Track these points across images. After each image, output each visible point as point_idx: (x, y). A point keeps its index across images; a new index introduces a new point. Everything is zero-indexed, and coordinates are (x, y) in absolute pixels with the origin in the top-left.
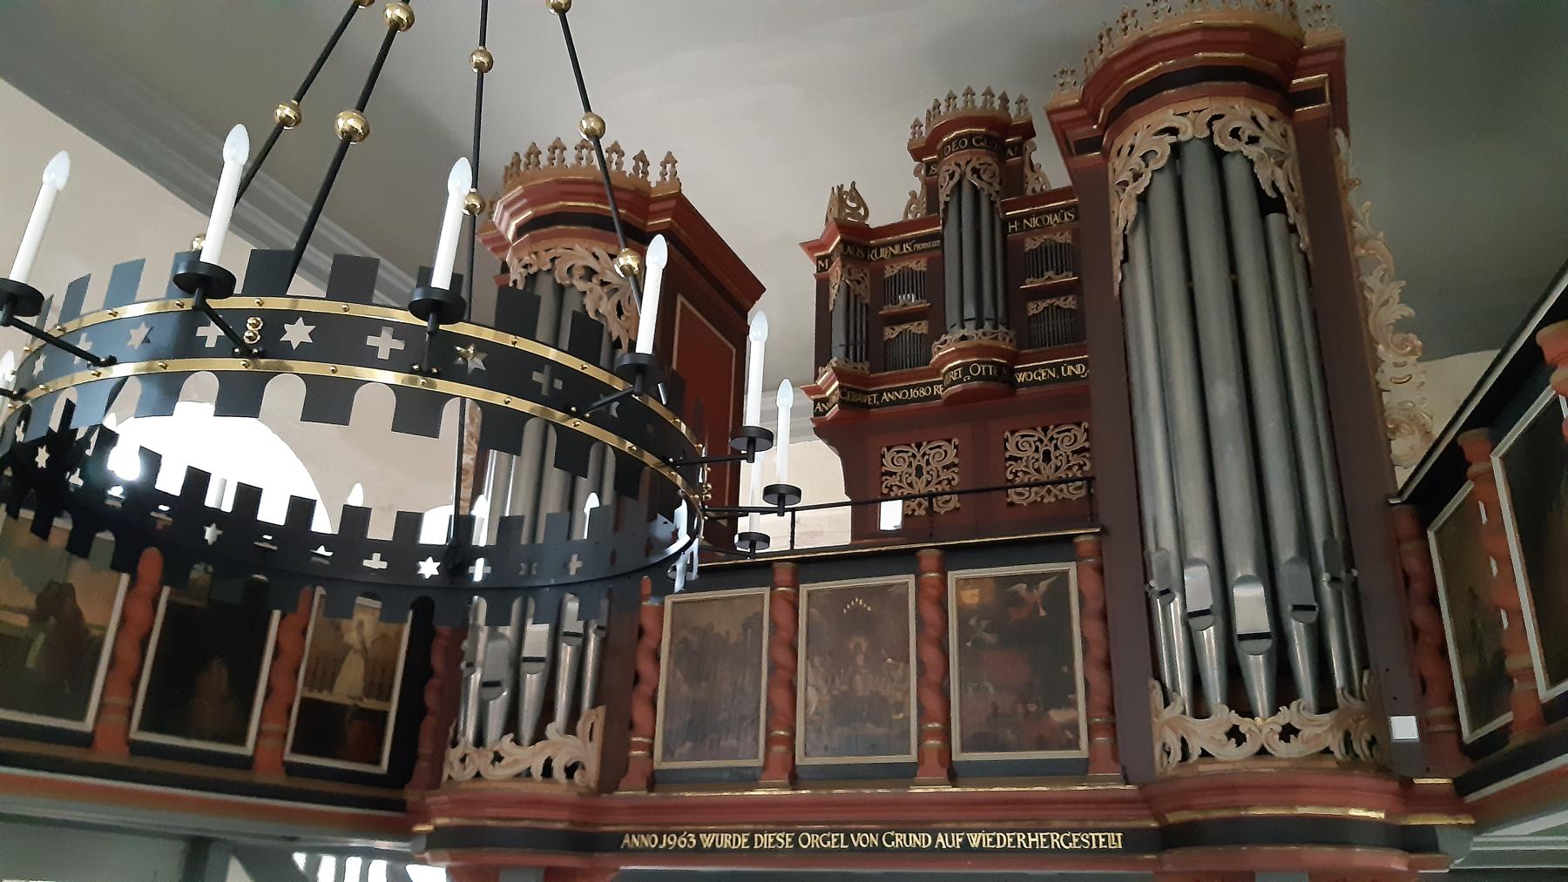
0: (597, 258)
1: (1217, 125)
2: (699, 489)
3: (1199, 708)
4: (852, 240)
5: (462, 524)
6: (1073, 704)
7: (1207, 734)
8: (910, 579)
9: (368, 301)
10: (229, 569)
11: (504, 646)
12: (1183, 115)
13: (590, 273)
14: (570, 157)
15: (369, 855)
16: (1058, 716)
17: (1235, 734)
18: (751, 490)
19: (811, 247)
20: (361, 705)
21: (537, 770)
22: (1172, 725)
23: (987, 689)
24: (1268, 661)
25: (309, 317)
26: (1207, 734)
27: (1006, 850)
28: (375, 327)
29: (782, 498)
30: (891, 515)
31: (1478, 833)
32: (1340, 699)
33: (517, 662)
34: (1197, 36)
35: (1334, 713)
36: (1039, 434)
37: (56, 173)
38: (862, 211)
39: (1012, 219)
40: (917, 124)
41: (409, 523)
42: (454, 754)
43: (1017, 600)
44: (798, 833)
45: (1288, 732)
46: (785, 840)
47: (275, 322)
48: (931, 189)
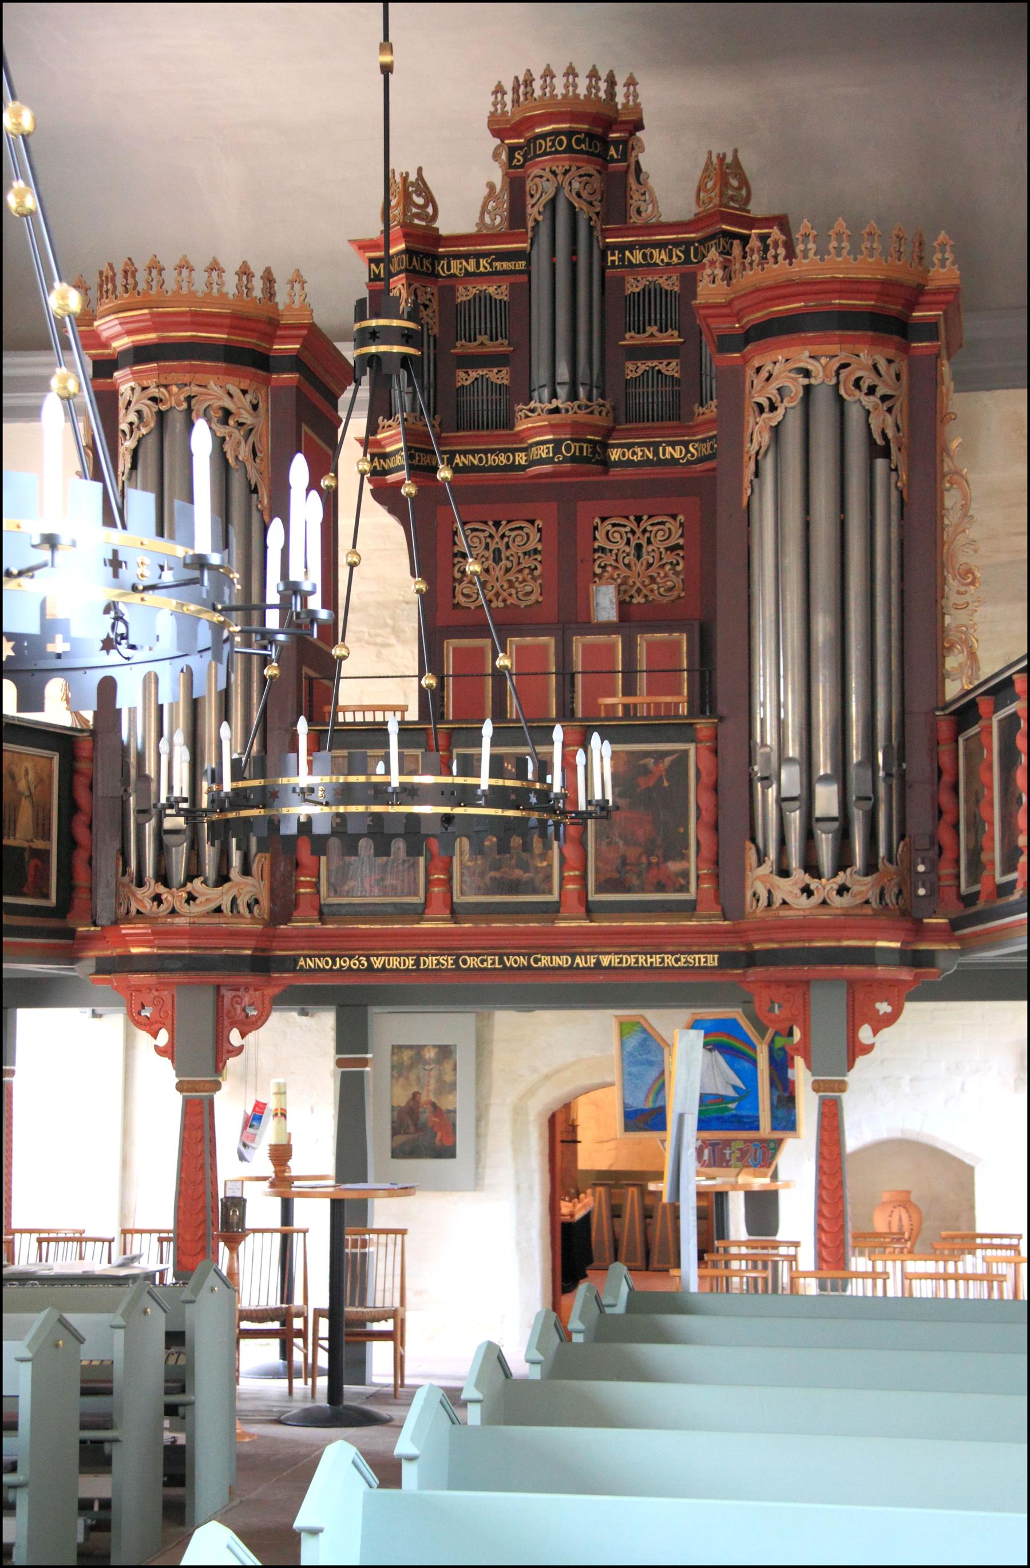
0: (230, 395)
1: (844, 373)
6: (685, 857)
7: (787, 889)
16: (674, 866)
20: (34, 846)
22: (760, 879)
23: (617, 843)
24: (835, 839)
26: (787, 889)
27: (629, 967)
31: (962, 955)
32: (880, 866)
34: (837, 286)
35: (874, 876)
36: (632, 524)
38: (430, 210)
39: (613, 247)
40: (499, 90)
43: (646, 771)
44: (459, 956)
45: (842, 890)
46: (447, 962)
48: (516, 189)
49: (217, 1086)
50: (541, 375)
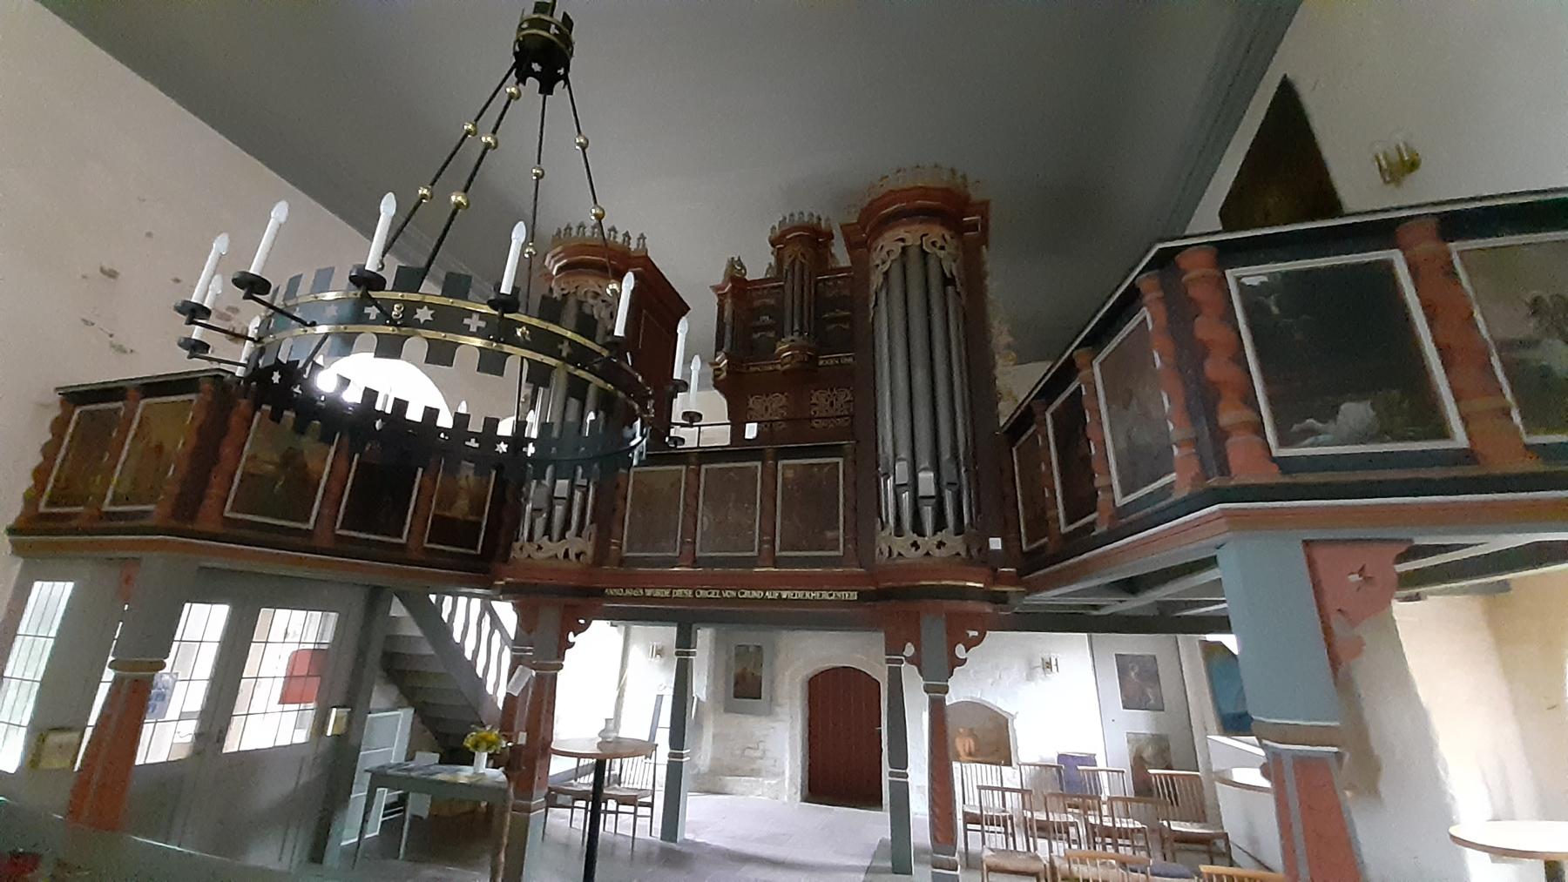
2: (648, 412)
3: (899, 531)
4: (737, 288)
5: (521, 425)
7: (901, 545)
8: (759, 464)
9: (465, 298)
10: (387, 441)
11: (544, 492)
12: (910, 234)
13: (596, 295)
14: (588, 234)
15: (470, 596)
16: (829, 534)
17: (915, 545)
18: (677, 416)
19: (716, 289)
21: (561, 556)
25: (431, 306)
26: (901, 545)
28: (470, 313)
29: (692, 418)
30: (751, 431)
33: (551, 499)
37: (279, 213)
41: (492, 424)
42: (517, 545)
45: (940, 545)
46: (689, 593)
47: (410, 308)
48: (779, 260)
49: (561, 667)
50: (787, 328)
